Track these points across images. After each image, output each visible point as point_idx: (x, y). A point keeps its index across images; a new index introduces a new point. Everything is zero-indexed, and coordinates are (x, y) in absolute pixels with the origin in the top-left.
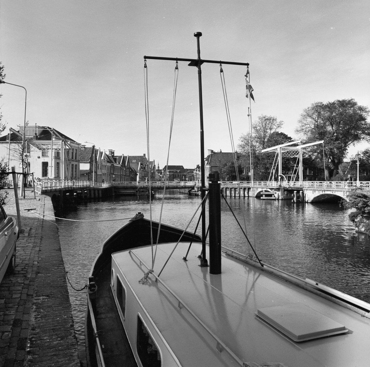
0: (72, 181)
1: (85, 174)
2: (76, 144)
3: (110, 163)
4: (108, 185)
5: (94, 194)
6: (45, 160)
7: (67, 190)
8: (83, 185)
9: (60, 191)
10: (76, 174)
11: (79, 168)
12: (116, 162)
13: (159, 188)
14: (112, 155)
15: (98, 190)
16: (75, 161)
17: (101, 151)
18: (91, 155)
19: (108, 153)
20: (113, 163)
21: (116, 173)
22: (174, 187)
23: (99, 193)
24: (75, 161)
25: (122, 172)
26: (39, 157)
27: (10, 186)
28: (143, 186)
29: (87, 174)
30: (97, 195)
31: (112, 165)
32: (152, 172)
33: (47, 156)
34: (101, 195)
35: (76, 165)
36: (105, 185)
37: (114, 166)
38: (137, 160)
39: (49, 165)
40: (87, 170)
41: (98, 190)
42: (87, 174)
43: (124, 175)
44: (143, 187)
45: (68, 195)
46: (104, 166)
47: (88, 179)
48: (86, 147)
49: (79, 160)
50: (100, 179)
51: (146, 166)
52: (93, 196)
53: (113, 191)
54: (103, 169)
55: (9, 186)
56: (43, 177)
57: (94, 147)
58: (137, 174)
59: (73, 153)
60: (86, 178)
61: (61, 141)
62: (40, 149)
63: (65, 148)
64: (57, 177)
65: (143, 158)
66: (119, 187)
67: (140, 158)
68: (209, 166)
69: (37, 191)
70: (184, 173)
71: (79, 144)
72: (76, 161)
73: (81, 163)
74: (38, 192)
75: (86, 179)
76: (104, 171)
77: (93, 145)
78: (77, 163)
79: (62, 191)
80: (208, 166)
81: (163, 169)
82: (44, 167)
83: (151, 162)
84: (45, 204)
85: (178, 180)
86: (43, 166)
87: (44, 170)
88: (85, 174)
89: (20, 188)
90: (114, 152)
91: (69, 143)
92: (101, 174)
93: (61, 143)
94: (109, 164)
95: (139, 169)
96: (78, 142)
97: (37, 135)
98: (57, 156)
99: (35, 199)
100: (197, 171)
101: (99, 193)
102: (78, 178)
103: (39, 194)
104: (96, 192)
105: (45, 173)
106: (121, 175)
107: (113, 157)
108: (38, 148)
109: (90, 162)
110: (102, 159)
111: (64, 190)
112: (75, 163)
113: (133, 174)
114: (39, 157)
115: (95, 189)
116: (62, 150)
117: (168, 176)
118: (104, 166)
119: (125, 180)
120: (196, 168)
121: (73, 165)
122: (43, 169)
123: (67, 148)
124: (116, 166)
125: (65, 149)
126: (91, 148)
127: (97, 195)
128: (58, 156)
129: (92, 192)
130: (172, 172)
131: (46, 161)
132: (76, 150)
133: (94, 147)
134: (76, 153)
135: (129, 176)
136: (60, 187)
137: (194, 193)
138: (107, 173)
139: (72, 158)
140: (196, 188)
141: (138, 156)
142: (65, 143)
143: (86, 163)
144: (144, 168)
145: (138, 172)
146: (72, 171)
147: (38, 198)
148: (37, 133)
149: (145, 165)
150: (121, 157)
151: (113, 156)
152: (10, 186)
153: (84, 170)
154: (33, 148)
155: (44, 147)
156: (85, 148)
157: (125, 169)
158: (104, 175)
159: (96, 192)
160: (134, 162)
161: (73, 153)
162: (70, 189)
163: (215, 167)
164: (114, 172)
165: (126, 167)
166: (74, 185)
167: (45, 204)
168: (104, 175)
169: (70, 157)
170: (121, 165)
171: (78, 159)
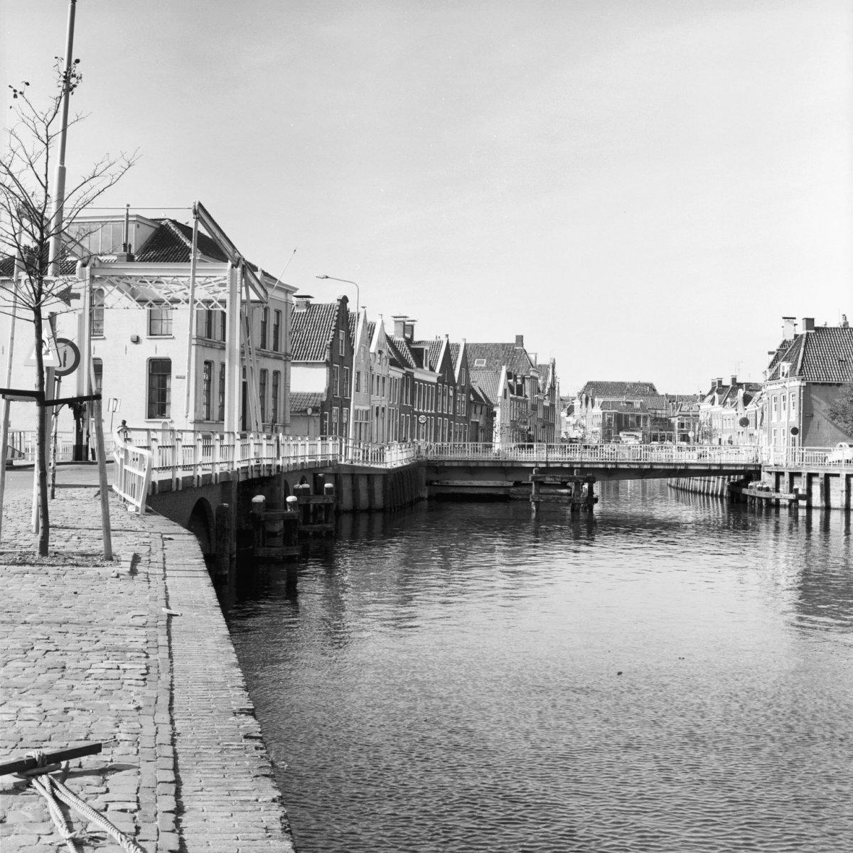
0: (274, 438)
1: (310, 411)
2: (278, 288)
3: (401, 367)
4: (405, 456)
5: (355, 491)
6: (161, 349)
7: (253, 480)
8: (310, 457)
9: (225, 483)
10: (275, 410)
11: (287, 386)
12: (420, 365)
13: (612, 469)
14: (404, 337)
15: (370, 476)
16: (275, 358)
17: (369, 320)
18: (332, 333)
19: (391, 330)
20: (409, 366)
21: (427, 409)
22: (675, 470)
23: (371, 492)
24: (272, 355)
25: (440, 406)
26: (138, 338)
27: (13, 456)
28: (547, 463)
29: (315, 410)
30: (364, 496)
31: (407, 374)
32: (547, 404)
33: (168, 336)
34: (379, 500)
35: (276, 373)
36: (396, 457)
37: (414, 380)
38: (489, 359)
39: (176, 370)
40: (315, 395)
41: (368, 475)
42: (315, 410)
43: (447, 416)
44: (544, 465)
45: (259, 504)
46: (378, 377)
47: (319, 430)
48: (312, 301)
49: (286, 355)
50: (363, 429)
51: (526, 381)
52: (347, 502)
53: (424, 481)
54: (375, 392)
55: (9, 457)
56: (149, 418)
57: (344, 300)
58: (494, 414)
59: (264, 324)
60: (312, 424)
61: (230, 263)
62: (142, 301)
63: (244, 297)
64: (209, 420)
65: (515, 352)
66: (446, 464)
67: (502, 353)
68: (798, 383)
69: (121, 493)
70: (659, 412)
71: (288, 290)
72: (277, 358)
73: (294, 364)
74: (129, 498)
75: (312, 431)
76: (381, 400)
77: (340, 295)
78: (279, 365)
79: (234, 488)
80: (793, 384)
81: (580, 394)
82: (156, 380)
83: (542, 369)
84: (170, 616)
85: (637, 437)
86: (151, 375)
87: (155, 392)
88: (310, 411)
89: (33, 466)
90: (412, 327)
91: (259, 277)
92: (367, 412)
93: (227, 274)
94: (397, 373)
95: (500, 393)
96: (284, 281)
97: (133, 251)
98: (203, 333)
99: (110, 557)
100: (713, 401)
101: (371, 492)
102: (285, 426)
103: (131, 509)
104: (363, 484)
105: (158, 404)
106: (436, 415)
107: (409, 347)
108: (133, 294)
109: (328, 364)
110: (373, 348)
111: (242, 478)
112: (271, 365)
113: (478, 410)
114: (137, 341)
115: (357, 472)
116: (231, 303)
117: (600, 420)
118: (378, 377)
119: (450, 434)
120: (711, 393)
121: (264, 372)
122: (151, 388)
123: (254, 296)
124: (420, 381)
125: (243, 302)
126: (332, 306)
127: (364, 496)
128: (209, 336)
129: (347, 484)
130: (614, 405)
131: (161, 354)
132: (278, 312)
133: (344, 300)
134: (277, 327)
135: (467, 419)
136: (225, 467)
137: (763, 494)
138: (390, 405)
139: (263, 346)
140: (770, 473)
141: (496, 345)
142: (244, 273)
143: (313, 365)
144: (520, 390)
145: (497, 405)
146: (262, 398)
147: (123, 547)
148: (132, 241)
149: (523, 379)
150: (439, 344)
151: (409, 341)
152: (13, 456)
153: (304, 395)
154: (114, 297)
155: (159, 293)
156: (308, 305)
157: (451, 393)
158: (377, 414)
159: (363, 484)
160: (479, 365)
161: (264, 324)
162: (266, 474)
163: (824, 387)
164: (412, 403)
165: (455, 385)
166: (278, 454)
167: (170, 616)
168: (377, 414)
169: (257, 341)
170: (438, 378)
171: (283, 351)
